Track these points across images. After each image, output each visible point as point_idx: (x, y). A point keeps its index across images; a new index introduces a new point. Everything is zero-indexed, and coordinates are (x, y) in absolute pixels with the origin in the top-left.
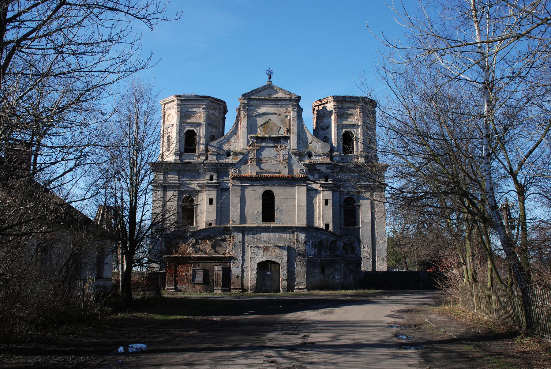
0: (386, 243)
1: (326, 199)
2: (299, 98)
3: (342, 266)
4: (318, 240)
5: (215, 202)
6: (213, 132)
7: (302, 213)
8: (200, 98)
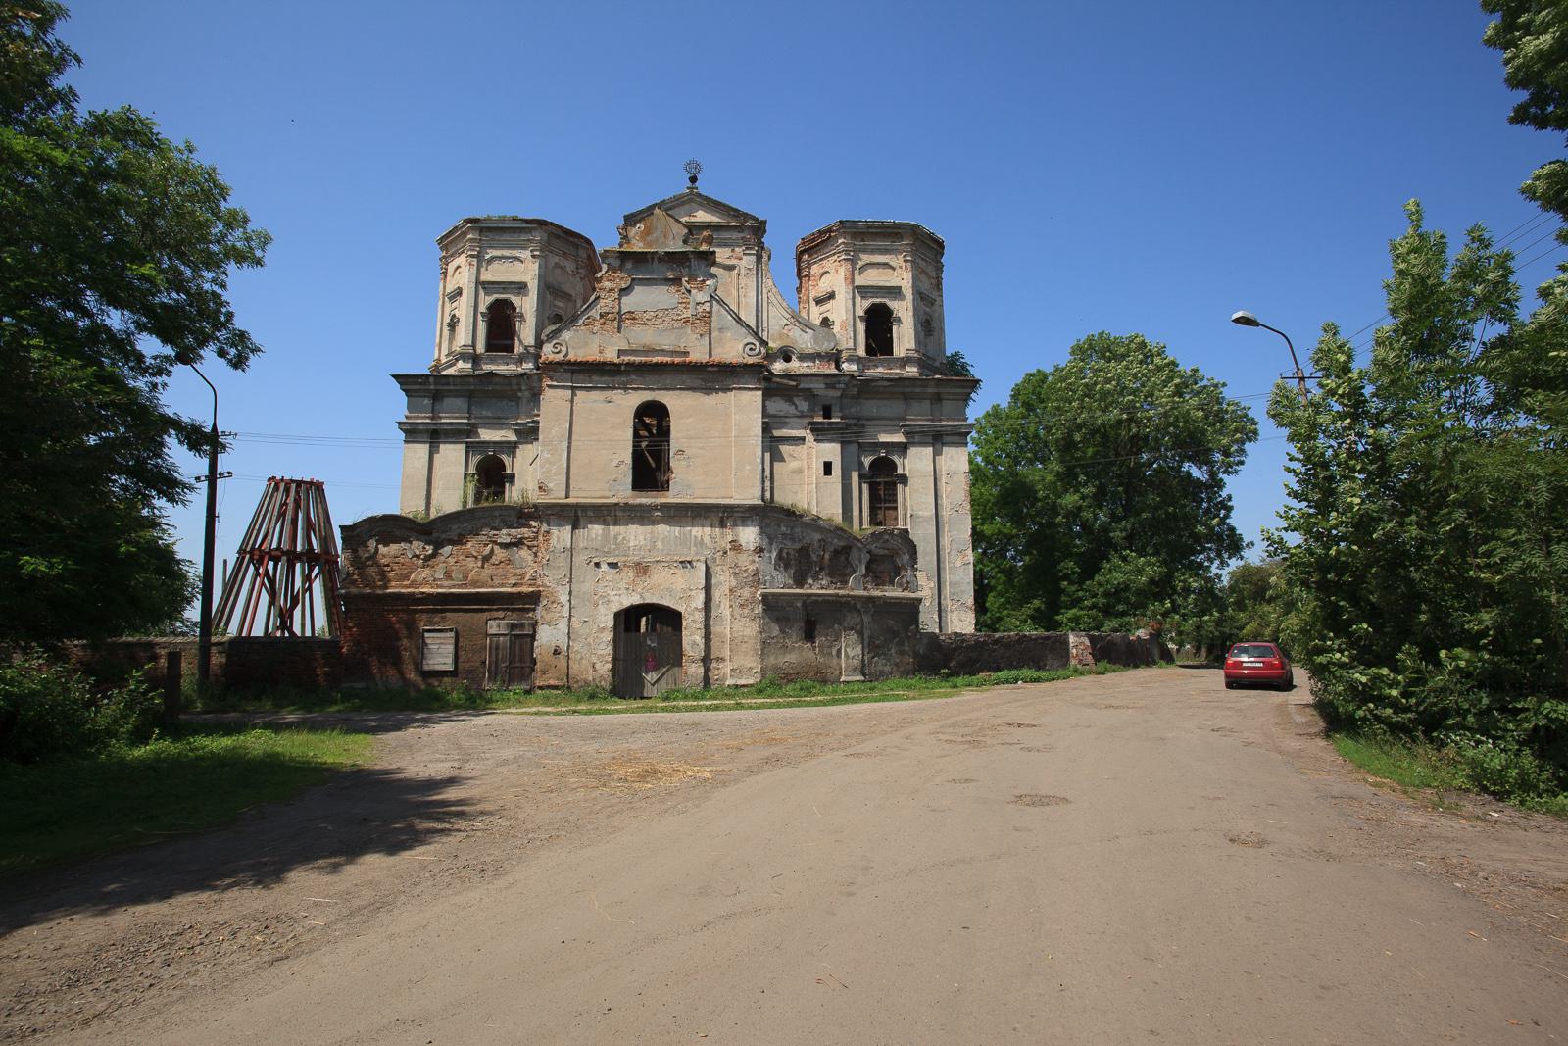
0: (972, 565)
3: (867, 619)
4: (797, 546)
6: (558, 307)
7: (748, 467)
8: (525, 226)
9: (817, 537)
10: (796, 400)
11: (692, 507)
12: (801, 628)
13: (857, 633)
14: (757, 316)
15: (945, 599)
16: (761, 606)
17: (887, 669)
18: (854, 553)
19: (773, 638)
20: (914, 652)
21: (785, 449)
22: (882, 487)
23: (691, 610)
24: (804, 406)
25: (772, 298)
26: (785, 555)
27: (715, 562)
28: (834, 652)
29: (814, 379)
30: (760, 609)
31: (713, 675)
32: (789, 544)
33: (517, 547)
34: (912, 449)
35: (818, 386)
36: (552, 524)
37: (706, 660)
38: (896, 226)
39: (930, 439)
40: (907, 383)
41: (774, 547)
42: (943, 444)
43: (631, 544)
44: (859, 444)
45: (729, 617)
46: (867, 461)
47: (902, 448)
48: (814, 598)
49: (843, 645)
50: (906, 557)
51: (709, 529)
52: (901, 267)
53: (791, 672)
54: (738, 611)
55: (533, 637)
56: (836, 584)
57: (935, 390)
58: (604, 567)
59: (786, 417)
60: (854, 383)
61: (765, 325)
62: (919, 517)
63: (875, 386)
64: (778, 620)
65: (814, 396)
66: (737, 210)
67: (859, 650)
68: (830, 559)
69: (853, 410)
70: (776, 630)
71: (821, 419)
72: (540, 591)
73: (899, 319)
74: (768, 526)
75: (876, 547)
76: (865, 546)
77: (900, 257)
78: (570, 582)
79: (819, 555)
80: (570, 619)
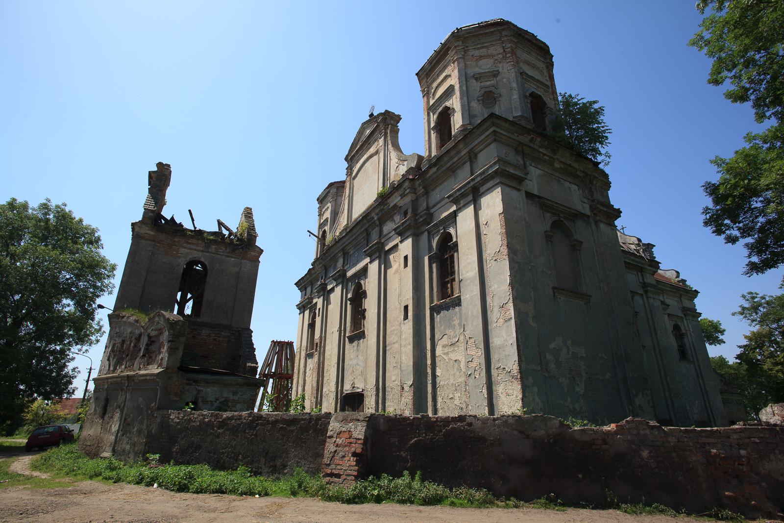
63: (430, 177)
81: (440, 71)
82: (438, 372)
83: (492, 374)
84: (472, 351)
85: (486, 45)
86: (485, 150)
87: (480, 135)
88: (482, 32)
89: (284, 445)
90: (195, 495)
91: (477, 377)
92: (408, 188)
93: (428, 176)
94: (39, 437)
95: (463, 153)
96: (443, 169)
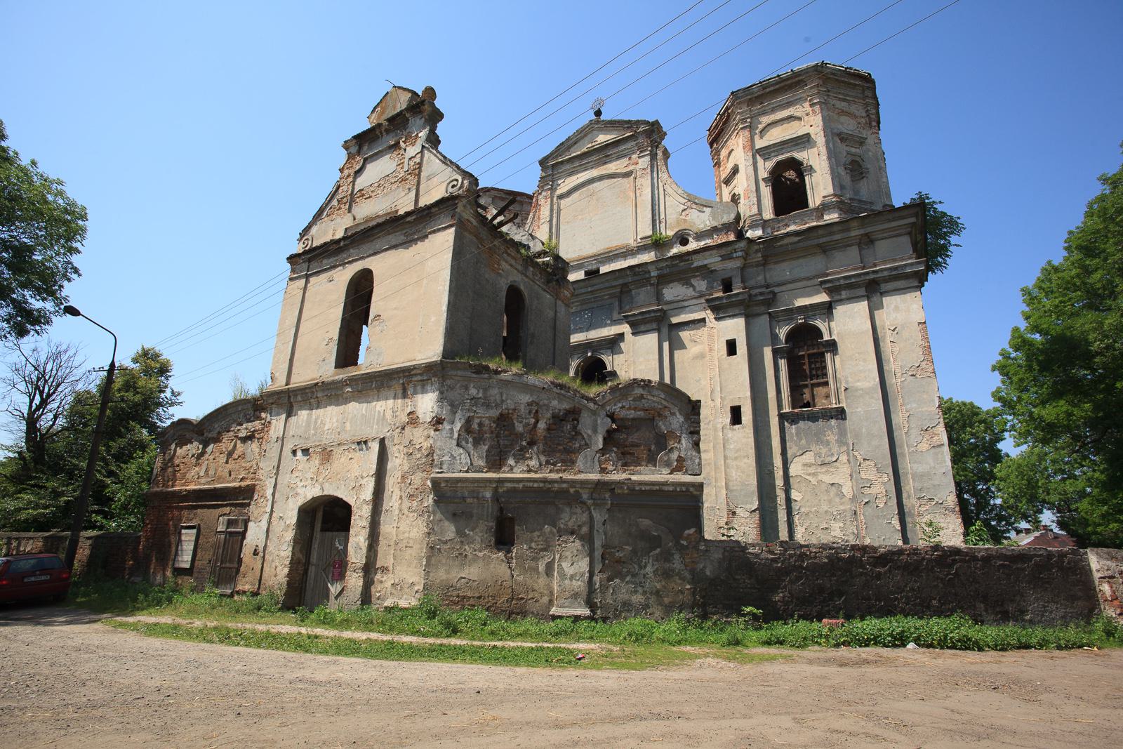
1: (730, 337)
2: (430, 92)
3: (599, 516)
4: (494, 413)
5: (747, 416)
9: (526, 398)
10: (694, 281)
11: (375, 377)
12: (490, 529)
13: (582, 538)
14: (653, 210)
15: (909, 497)
16: (431, 496)
17: (638, 599)
18: (585, 420)
19: (446, 542)
20: (693, 572)
21: (685, 335)
22: (806, 360)
23: (360, 501)
24: (701, 285)
25: (669, 190)
26: (475, 426)
27: (393, 440)
28: (542, 567)
29: (708, 253)
30: (431, 501)
31: (375, 590)
32: (481, 411)
33: (251, 440)
34: (838, 307)
35: (712, 260)
36: (273, 414)
37: (369, 569)
38: (795, 74)
39: (862, 291)
40: (821, 232)
41: (458, 415)
42: (882, 294)
43: (326, 428)
44: (770, 314)
45: (397, 512)
46: (782, 332)
47: (827, 310)
48: (509, 485)
49: (557, 557)
50: (677, 420)
51: (392, 401)
52: (807, 114)
53: (469, 594)
54: (406, 503)
55: (243, 535)
56: (554, 464)
57: (862, 231)
58: (299, 453)
59: (683, 301)
60: (756, 247)
61: (662, 216)
62: (857, 390)
63: (781, 246)
64: (454, 516)
65: (712, 271)
66: (629, 122)
67: (584, 565)
68: (549, 429)
69: (760, 278)
70: (450, 531)
71: (720, 294)
72: (254, 485)
73: (811, 168)
74: (451, 388)
75: (623, 407)
76: (603, 406)
77: (807, 105)
78: (277, 474)
79: (528, 424)
80: (271, 515)
81: (779, 105)
82: (795, 495)
83: (904, 503)
84: (868, 473)
85: (848, 98)
86: (887, 240)
87: (890, 221)
88: (846, 80)
89: (1013, 586)
90: (1001, 653)
91: (881, 505)
92: (741, 251)
93: (778, 244)
94: (26, 580)
95: (853, 233)
96: (809, 243)
